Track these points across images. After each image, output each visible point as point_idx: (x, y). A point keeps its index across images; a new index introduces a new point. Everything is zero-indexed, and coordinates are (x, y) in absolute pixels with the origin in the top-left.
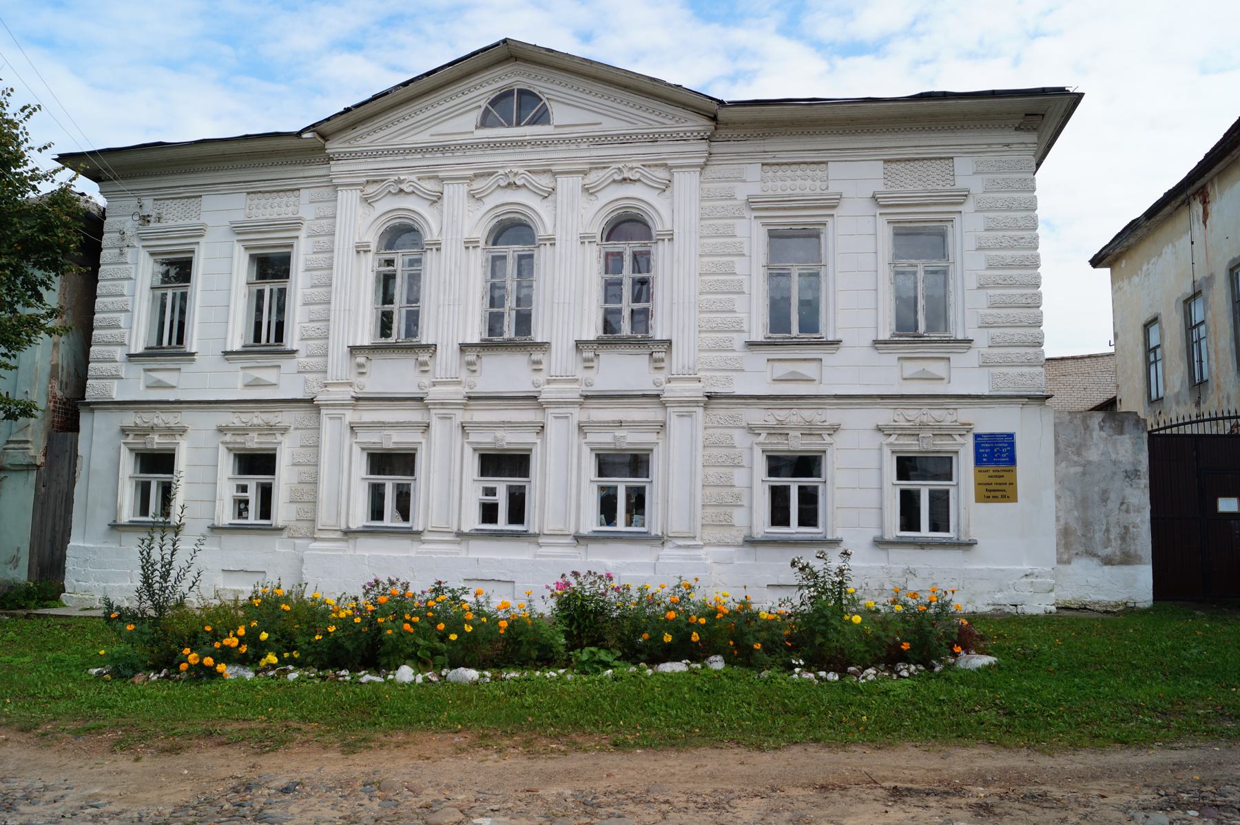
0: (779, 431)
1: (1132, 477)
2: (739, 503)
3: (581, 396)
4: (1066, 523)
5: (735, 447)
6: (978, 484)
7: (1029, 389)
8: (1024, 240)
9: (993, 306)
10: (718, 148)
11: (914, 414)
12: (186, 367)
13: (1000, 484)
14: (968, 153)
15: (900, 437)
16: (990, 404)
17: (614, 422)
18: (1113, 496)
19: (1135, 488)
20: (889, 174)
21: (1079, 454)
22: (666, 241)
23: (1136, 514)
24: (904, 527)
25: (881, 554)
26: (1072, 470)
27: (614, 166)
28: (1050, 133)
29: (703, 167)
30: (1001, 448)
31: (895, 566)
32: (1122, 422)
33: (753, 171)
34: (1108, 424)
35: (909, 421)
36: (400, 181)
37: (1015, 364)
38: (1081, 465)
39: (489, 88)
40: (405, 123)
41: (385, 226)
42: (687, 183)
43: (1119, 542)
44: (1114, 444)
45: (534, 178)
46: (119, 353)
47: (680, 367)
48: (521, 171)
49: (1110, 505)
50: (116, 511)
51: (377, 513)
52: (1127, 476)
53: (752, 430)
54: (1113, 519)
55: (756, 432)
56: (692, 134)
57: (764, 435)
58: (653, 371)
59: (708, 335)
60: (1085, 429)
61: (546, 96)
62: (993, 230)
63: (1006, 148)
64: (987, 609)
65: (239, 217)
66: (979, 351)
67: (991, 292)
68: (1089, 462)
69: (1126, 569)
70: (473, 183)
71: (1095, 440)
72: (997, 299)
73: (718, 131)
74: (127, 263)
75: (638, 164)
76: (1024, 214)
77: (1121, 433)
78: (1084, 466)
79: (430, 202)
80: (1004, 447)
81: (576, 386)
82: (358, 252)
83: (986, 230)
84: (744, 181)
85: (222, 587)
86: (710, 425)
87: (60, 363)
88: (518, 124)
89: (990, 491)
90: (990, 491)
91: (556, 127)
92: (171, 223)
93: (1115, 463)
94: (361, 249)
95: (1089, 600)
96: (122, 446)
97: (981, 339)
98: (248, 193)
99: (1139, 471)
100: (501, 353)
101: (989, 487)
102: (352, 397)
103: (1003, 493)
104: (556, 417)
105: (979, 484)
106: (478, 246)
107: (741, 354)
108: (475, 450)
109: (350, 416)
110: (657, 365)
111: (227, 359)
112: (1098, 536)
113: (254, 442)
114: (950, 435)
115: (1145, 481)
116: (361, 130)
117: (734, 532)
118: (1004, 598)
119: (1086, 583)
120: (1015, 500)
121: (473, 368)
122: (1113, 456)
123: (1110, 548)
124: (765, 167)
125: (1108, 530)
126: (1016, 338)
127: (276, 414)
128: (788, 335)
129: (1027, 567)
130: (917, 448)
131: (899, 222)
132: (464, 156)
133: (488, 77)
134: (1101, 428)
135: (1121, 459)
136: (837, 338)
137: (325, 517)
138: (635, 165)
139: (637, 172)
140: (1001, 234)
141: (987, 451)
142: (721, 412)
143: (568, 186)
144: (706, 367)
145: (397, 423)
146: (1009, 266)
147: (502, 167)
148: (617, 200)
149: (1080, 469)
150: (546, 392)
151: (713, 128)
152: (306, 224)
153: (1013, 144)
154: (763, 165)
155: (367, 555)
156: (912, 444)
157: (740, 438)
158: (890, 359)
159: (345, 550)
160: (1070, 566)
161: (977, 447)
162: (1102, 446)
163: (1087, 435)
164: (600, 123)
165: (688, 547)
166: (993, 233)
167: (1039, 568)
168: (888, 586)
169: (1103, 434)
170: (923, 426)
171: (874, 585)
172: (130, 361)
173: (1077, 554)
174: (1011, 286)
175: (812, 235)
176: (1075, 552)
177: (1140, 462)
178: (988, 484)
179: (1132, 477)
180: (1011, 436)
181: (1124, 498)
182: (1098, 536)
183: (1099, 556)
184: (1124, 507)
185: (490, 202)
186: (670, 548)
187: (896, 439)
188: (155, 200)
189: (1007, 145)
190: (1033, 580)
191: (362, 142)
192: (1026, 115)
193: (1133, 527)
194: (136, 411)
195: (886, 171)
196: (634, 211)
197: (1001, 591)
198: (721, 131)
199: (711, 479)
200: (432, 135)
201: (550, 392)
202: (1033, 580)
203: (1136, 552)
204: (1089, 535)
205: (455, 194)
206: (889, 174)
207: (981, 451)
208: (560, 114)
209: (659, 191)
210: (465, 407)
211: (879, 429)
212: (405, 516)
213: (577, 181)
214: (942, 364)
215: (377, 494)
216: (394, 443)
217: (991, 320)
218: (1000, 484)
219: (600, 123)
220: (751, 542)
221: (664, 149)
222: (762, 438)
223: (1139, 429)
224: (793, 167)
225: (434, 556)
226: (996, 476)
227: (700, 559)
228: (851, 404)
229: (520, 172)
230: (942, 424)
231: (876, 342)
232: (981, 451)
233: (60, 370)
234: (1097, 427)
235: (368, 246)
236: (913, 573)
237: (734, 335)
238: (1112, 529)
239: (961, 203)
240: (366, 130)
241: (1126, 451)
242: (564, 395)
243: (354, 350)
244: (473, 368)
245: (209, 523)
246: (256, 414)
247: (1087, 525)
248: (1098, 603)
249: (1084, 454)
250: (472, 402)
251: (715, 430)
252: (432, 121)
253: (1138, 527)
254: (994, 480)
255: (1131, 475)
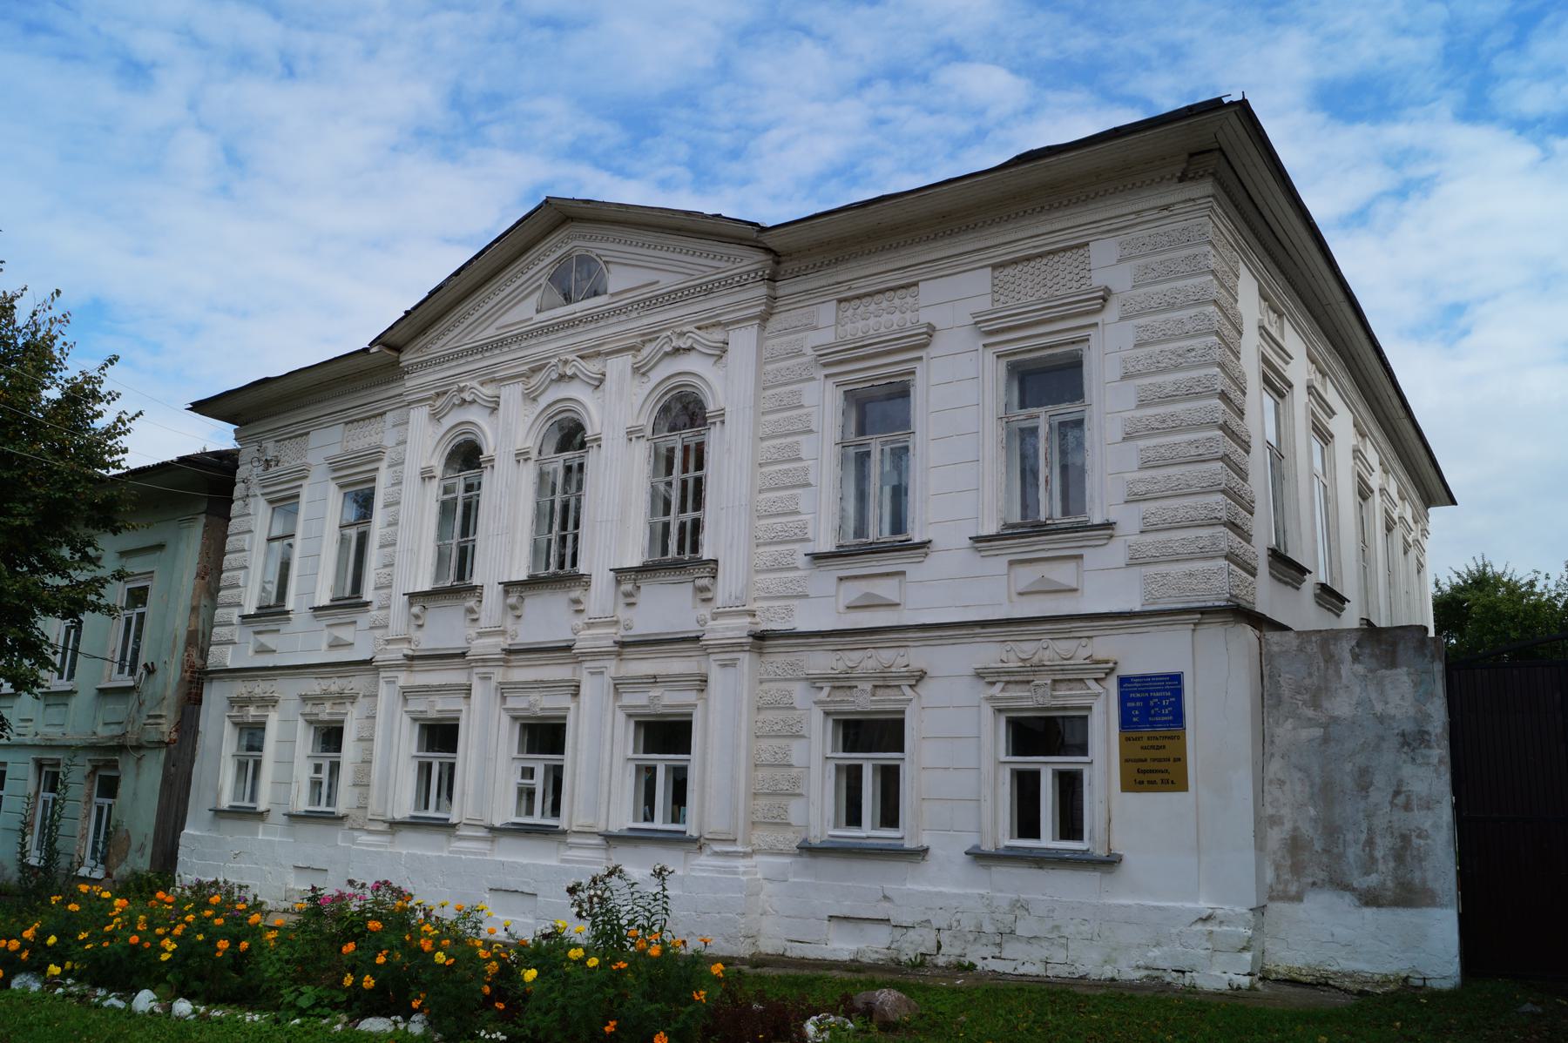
0: (842, 682)
1: (1415, 744)
2: (797, 792)
3: (615, 642)
4: (1295, 829)
5: (794, 708)
6: (1125, 760)
7: (1201, 598)
8: (1193, 354)
9: (1146, 465)
10: (784, 288)
11: (1028, 649)
12: (284, 628)
13: (1160, 760)
14: (1108, 231)
15: (1010, 686)
17: (647, 677)
18: (1379, 780)
19: (1420, 765)
20: (1001, 284)
21: (1316, 705)
22: (718, 424)
23: (1423, 813)
25: (979, 873)
26: (1305, 734)
27: (664, 334)
29: (764, 318)
31: (999, 895)
32: (1394, 645)
33: (826, 312)
34: (1367, 651)
36: (461, 390)
37: (1179, 557)
38: (1320, 725)
40: (471, 319)
41: (451, 445)
42: (743, 341)
43: (1392, 864)
44: (1380, 685)
45: (583, 363)
46: (234, 615)
47: (727, 595)
48: (570, 357)
49: (1375, 796)
50: (218, 796)
51: (1027, 825)
52: (1405, 743)
53: (814, 681)
54: (1380, 822)
55: (818, 685)
57: (826, 691)
58: (699, 604)
59: (767, 549)
60: (1326, 661)
61: (604, 259)
63: (1166, 213)
64: (1137, 975)
65: (336, 450)
66: (1126, 541)
67: (1142, 443)
68: (1335, 720)
69: (1406, 915)
70: (531, 380)
71: (1344, 681)
72: (1151, 454)
73: (782, 265)
74: (249, 514)
76: (1192, 312)
77: (1392, 664)
78: (1326, 727)
79: (489, 411)
80: (1168, 697)
81: (614, 630)
82: (424, 479)
83: (1136, 346)
84: (816, 328)
85: (292, 886)
86: (765, 677)
87: (200, 628)
89: (1144, 772)
90: (1144, 772)
91: (612, 295)
92: (286, 465)
93: (1381, 719)
94: (426, 476)
95: (1335, 968)
96: (227, 719)
97: (1129, 520)
98: (347, 423)
99: (1427, 733)
100: (540, 592)
101: (1143, 766)
102: (405, 656)
103: (1165, 776)
104: (592, 673)
105: (1127, 761)
106: (529, 459)
107: (808, 572)
108: (630, 716)
109: (404, 679)
110: (704, 595)
112: (1353, 853)
113: (864, 701)
114: (1082, 680)
115: (1439, 752)
116: (432, 334)
117: (790, 835)
118: (1161, 957)
119: (1330, 939)
120: (1183, 787)
121: (518, 613)
122: (1379, 708)
123: (1374, 875)
124: (843, 305)
125: (1370, 843)
126: (1181, 513)
127: (350, 679)
128: (864, 540)
129: (1204, 905)
130: (1030, 704)
131: (1015, 354)
132: (521, 349)
133: (543, 249)
134: (1356, 658)
135: (1392, 712)
136: (925, 538)
137: (374, 807)
138: (685, 329)
139: (689, 337)
140: (1157, 348)
141: (1138, 704)
142: (778, 659)
143: (618, 367)
144: (763, 594)
145: (440, 686)
146: (1170, 398)
147: (554, 356)
148: (669, 378)
149: (1317, 732)
150: (581, 640)
151: (774, 262)
152: (388, 451)
153: (1173, 204)
154: (840, 301)
155: (404, 852)
156: (1021, 698)
157: (799, 692)
159: (386, 847)
160: (1302, 906)
161: (1124, 698)
162: (1358, 690)
163: (1331, 672)
164: (657, 282)
165: (726, 854)
167: (1227, 907)
168: (988, 928)
169: (1359, 668)
170: (1038, 668)
171: (968, 924)
172: (243, 623)
173: (1314, 884)
174: (1175, 429)
175: (900, 392)
176: (1310, 880)
177: (1430, 716)
179: (1415, 744)
180: (1176, 678)
181: (1400, 782)
182: (1353, 853)
183: (1354, 890)
184: (1401, 800)
186: (708, 856)
187: (1003, 690)
188: (277, 441)
189: (1166, 208)
190: (1216, 929)
191: (435, 348)
192: (1191, 155)
193: (1419, 836)
194: (244, 679)
195: (996, 282)
196: (689, 389)
197: (1158, 945)
198: (786, 264)
199: (764, 756)
200: (497, 329)
201: (585, 640)
202: (1216, 929)
203: (1424, 881)
204: (1335, 851)
205: (511, 395)
206: (1001, 284)
207: (1129, 704)
209: (715, 358)
210: (409, 668)
211: (980, 675)
213: (625, 361)
214: (1070, 566)
215: (1026, 786)
216: (541, 709)
217: (1141, 488)
218: (1160, 760)
219: (657, 282)
220: (809, 850)
221: (718, 302)
222: (823, 695)
223: (1425, 656)
224: (876, 298)
225: (463, 857)
227: (735, 873)
228: (941, 637)
229: (571, 359)
230: (1072, 662)
231: (977, 539)
232: (1129, 704)
233: (200, 636)
234: (1347, 656)
235: (431, 471)
236: (1025, 907)
237: (796, 546)
238: (1378, 840)
240: (435, 334)
241: (1403, 698)
242: (598, 643)
243: (413, 597)
244: (518, 613)
245: (970, 841)
246: (333, 680)
247: (1332, 832)
248: (1350, 976)
249: (1326, 704)
250: (512, 657)
251: (772, 684)
252: (497, 311)
253: (1427, 837)
255: (1413, 741)
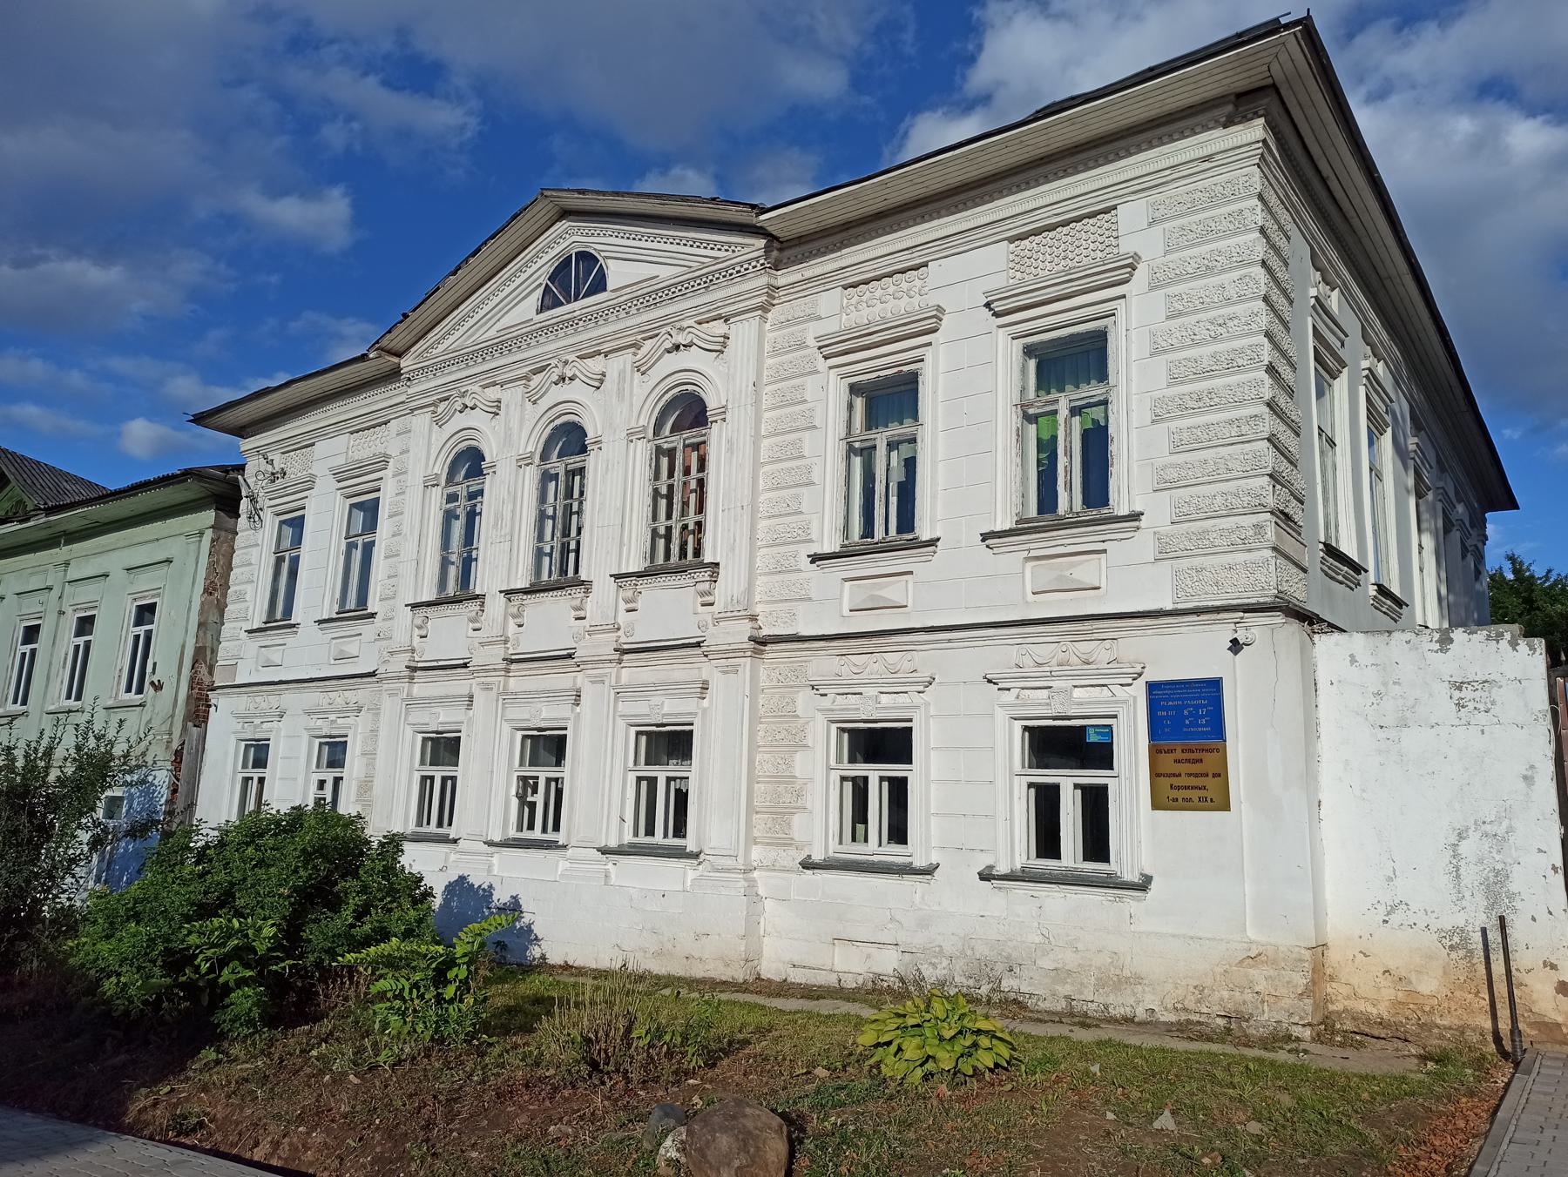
8: (1236, 322)
13: (1196, 776)
16: (1169, 626)
24: (1088, 856)
27: (663, 330)
28: (1333, 128)
29: (765, 308)
30: (1197, 707)
35: (1040, 665)
39: (546, 258)
55: (821, 691)
56: (758, 262)
61: (603, 254)
62: (1181, 314)
63: (1207, 165)
75: (691, 322)
83: (1168, 318)
88: (576, 300)
89: (1178, 788)
90: (1178, 788)
97: (1158, 513)
103: (1202, 793)
111: (321, 629)
140: (1193, 319)
141: (1170, 713)
152: (391, 461)
158: (1010, 558)
166: (1180, 321)
178: (1174, 775)
185: (545, 403)
188: (283, 453)
208: (618, 274)
209: (715, 354)
212: (680, 829)
213: (627, 358)
217: (1172, 474)
226: (1188, 761)
239: (1126, 281)
254: (1184, 768)
